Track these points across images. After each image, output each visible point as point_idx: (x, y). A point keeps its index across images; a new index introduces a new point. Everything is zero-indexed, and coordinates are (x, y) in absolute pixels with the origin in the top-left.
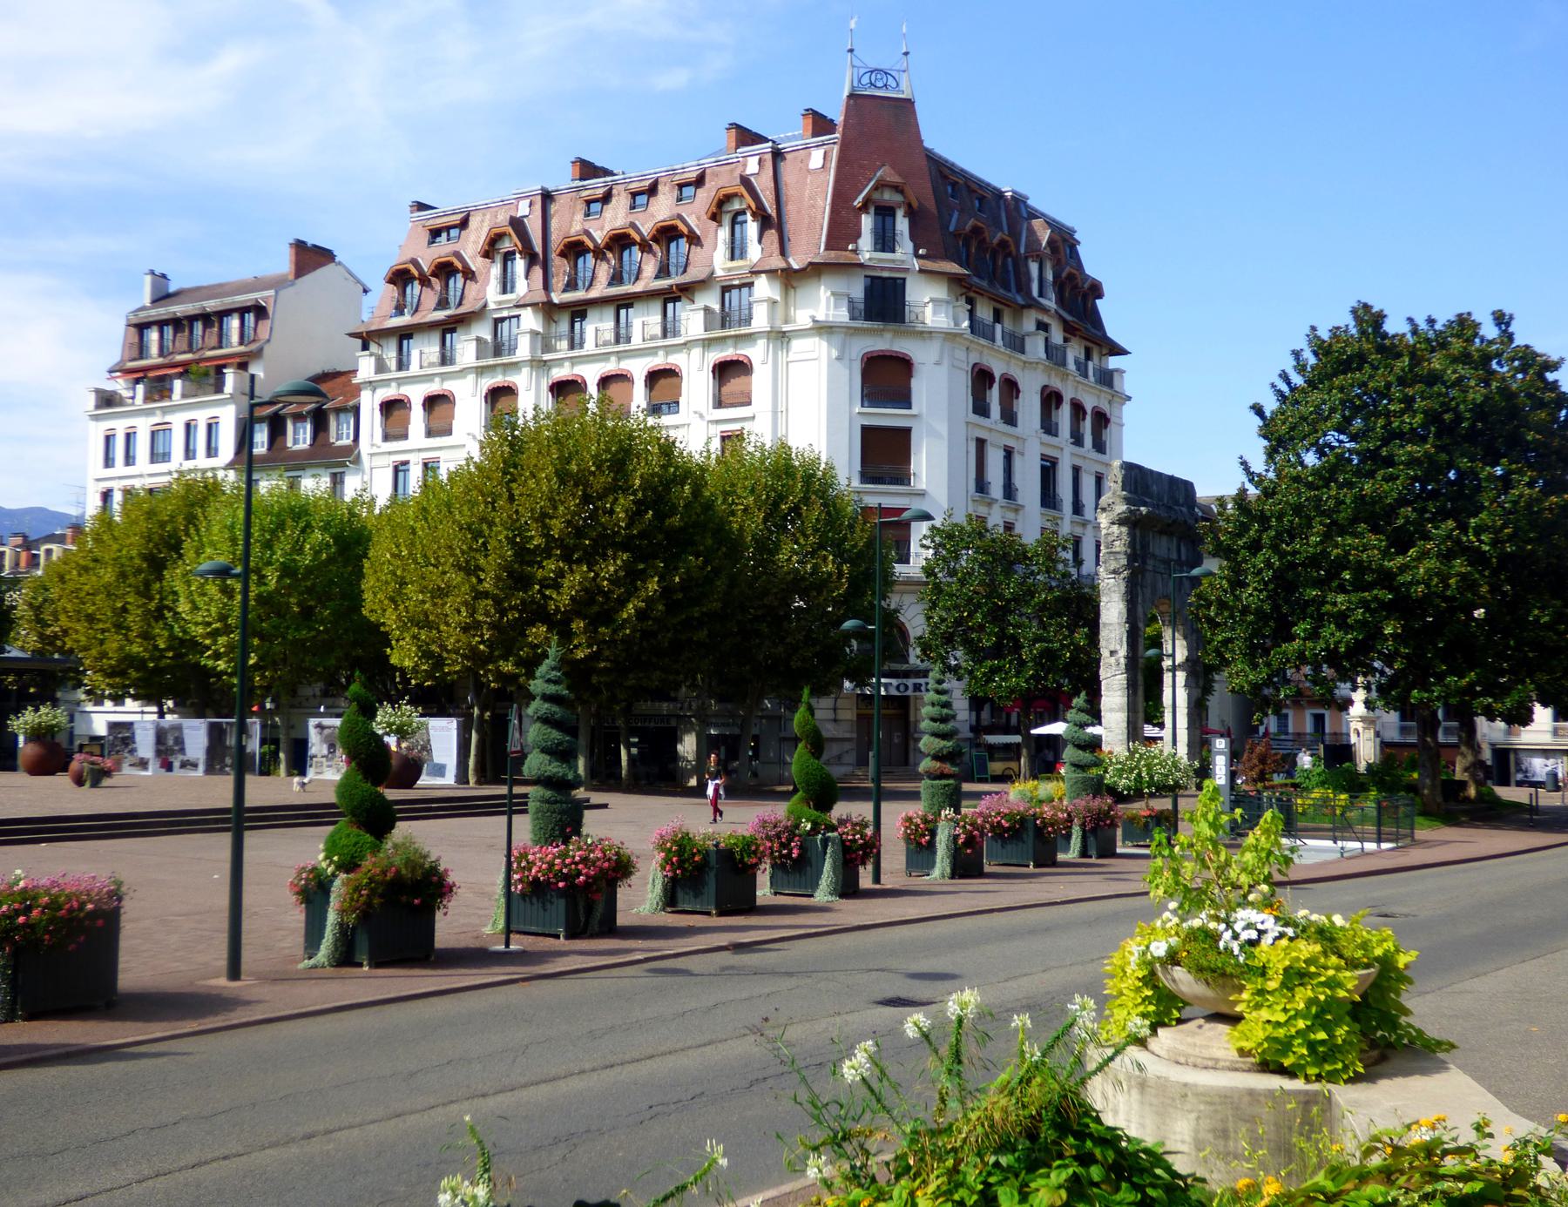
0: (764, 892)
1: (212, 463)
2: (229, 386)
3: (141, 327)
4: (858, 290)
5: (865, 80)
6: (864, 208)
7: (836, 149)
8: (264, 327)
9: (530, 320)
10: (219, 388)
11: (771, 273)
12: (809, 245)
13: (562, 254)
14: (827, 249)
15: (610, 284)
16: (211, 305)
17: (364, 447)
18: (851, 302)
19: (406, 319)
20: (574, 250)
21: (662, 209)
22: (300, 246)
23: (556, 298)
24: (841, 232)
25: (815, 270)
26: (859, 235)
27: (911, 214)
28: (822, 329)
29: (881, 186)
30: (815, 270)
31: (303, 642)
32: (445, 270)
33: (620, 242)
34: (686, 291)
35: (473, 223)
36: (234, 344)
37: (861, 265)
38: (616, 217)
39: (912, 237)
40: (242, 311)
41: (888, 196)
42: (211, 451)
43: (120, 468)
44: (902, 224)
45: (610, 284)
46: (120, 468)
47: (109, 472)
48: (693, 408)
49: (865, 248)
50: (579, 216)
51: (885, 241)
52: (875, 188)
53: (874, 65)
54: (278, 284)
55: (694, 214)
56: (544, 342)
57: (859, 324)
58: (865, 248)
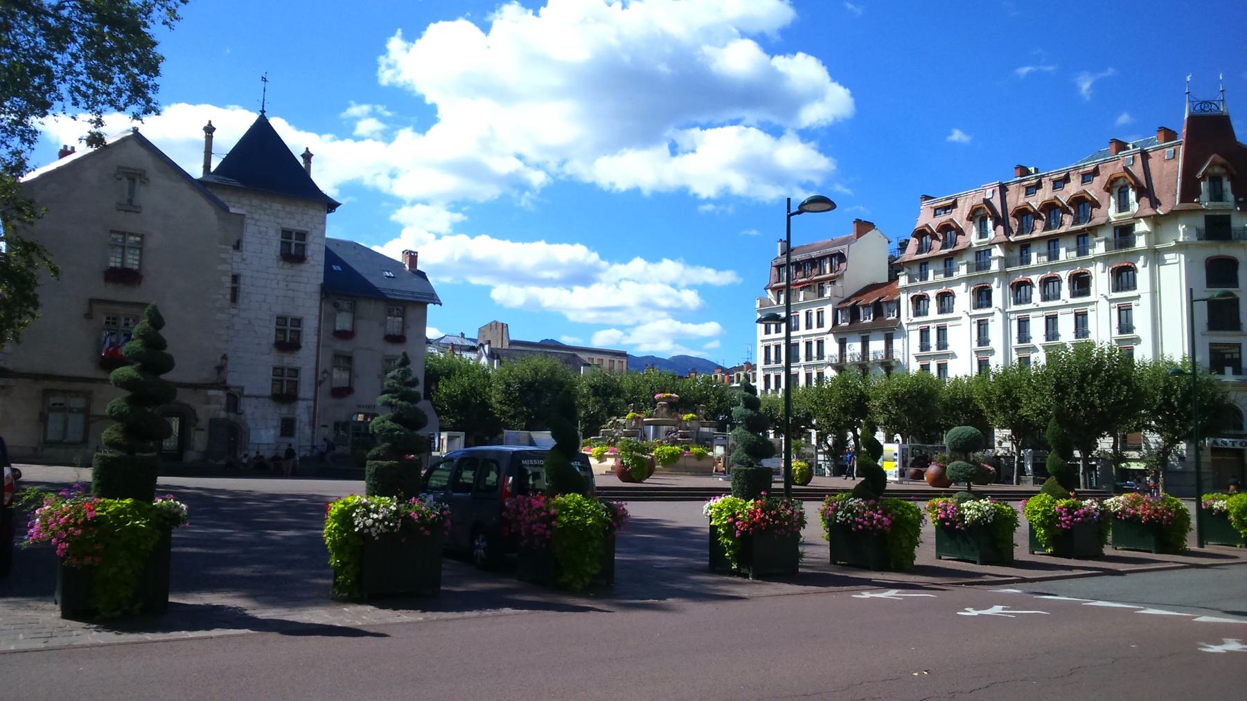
0: (1191, 544)
1: (778, 336)
2: (828, 294)
3: (779, 267)
4: (1200, 222)
5: (1198, 108)
6: (1203, 178)
7: (1182, 148)
8: (843, 266)
9: (997, 252)
10: (821, 294)
11: (1146, 218)
12: (1170, 199)
13: (1014, 216)
14: (1182, 201)
15: (1044, 230)
16: (814, 254)
17: (904, 320)
18: (1198, 230)
19: (925, 255)
20: (1023, 213)
21: (1074, 187)
22: (858, 222)
23: (1012, 239)
24: (1189, 190)
25: (1174, 215)
26: (1200, 193)
27: (1232, 179)
28: (1180, 248)
29: (1212, 165)
30: (1174, 215)
31: (1112, 386)
32: (945, 228)
33: (1051, 208)
34: (1094, 230)
35: (960, 204)
36: (828, 273)
37: (1203, 210)
38: (1045, 194)
39: (1233, 192)
40: (832, 256)
41: (1217, 170)
42: (820, 325)
43: (815, 330)
44: (1227, 185)
45: (1044, 230)
46: (815, 330)
47: (768, 337)
48: (1099, 292)
49: (1205, 201)
50: (1022, 195)
51: (1217, 195)
52: (1210, 166)
53: (1202, 99)
54: (847, 241)
55: (1094, 189)
56: (1006, 262)
57: (1203, 242)
58: (1205, 201)
